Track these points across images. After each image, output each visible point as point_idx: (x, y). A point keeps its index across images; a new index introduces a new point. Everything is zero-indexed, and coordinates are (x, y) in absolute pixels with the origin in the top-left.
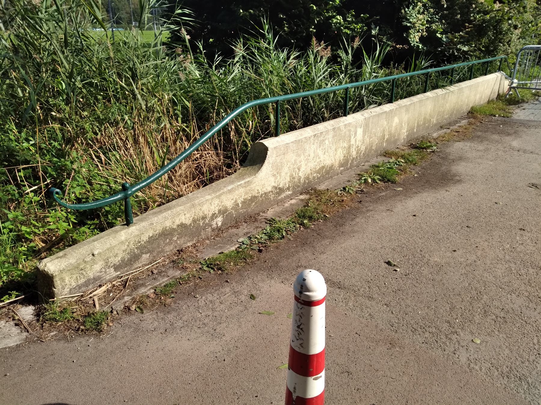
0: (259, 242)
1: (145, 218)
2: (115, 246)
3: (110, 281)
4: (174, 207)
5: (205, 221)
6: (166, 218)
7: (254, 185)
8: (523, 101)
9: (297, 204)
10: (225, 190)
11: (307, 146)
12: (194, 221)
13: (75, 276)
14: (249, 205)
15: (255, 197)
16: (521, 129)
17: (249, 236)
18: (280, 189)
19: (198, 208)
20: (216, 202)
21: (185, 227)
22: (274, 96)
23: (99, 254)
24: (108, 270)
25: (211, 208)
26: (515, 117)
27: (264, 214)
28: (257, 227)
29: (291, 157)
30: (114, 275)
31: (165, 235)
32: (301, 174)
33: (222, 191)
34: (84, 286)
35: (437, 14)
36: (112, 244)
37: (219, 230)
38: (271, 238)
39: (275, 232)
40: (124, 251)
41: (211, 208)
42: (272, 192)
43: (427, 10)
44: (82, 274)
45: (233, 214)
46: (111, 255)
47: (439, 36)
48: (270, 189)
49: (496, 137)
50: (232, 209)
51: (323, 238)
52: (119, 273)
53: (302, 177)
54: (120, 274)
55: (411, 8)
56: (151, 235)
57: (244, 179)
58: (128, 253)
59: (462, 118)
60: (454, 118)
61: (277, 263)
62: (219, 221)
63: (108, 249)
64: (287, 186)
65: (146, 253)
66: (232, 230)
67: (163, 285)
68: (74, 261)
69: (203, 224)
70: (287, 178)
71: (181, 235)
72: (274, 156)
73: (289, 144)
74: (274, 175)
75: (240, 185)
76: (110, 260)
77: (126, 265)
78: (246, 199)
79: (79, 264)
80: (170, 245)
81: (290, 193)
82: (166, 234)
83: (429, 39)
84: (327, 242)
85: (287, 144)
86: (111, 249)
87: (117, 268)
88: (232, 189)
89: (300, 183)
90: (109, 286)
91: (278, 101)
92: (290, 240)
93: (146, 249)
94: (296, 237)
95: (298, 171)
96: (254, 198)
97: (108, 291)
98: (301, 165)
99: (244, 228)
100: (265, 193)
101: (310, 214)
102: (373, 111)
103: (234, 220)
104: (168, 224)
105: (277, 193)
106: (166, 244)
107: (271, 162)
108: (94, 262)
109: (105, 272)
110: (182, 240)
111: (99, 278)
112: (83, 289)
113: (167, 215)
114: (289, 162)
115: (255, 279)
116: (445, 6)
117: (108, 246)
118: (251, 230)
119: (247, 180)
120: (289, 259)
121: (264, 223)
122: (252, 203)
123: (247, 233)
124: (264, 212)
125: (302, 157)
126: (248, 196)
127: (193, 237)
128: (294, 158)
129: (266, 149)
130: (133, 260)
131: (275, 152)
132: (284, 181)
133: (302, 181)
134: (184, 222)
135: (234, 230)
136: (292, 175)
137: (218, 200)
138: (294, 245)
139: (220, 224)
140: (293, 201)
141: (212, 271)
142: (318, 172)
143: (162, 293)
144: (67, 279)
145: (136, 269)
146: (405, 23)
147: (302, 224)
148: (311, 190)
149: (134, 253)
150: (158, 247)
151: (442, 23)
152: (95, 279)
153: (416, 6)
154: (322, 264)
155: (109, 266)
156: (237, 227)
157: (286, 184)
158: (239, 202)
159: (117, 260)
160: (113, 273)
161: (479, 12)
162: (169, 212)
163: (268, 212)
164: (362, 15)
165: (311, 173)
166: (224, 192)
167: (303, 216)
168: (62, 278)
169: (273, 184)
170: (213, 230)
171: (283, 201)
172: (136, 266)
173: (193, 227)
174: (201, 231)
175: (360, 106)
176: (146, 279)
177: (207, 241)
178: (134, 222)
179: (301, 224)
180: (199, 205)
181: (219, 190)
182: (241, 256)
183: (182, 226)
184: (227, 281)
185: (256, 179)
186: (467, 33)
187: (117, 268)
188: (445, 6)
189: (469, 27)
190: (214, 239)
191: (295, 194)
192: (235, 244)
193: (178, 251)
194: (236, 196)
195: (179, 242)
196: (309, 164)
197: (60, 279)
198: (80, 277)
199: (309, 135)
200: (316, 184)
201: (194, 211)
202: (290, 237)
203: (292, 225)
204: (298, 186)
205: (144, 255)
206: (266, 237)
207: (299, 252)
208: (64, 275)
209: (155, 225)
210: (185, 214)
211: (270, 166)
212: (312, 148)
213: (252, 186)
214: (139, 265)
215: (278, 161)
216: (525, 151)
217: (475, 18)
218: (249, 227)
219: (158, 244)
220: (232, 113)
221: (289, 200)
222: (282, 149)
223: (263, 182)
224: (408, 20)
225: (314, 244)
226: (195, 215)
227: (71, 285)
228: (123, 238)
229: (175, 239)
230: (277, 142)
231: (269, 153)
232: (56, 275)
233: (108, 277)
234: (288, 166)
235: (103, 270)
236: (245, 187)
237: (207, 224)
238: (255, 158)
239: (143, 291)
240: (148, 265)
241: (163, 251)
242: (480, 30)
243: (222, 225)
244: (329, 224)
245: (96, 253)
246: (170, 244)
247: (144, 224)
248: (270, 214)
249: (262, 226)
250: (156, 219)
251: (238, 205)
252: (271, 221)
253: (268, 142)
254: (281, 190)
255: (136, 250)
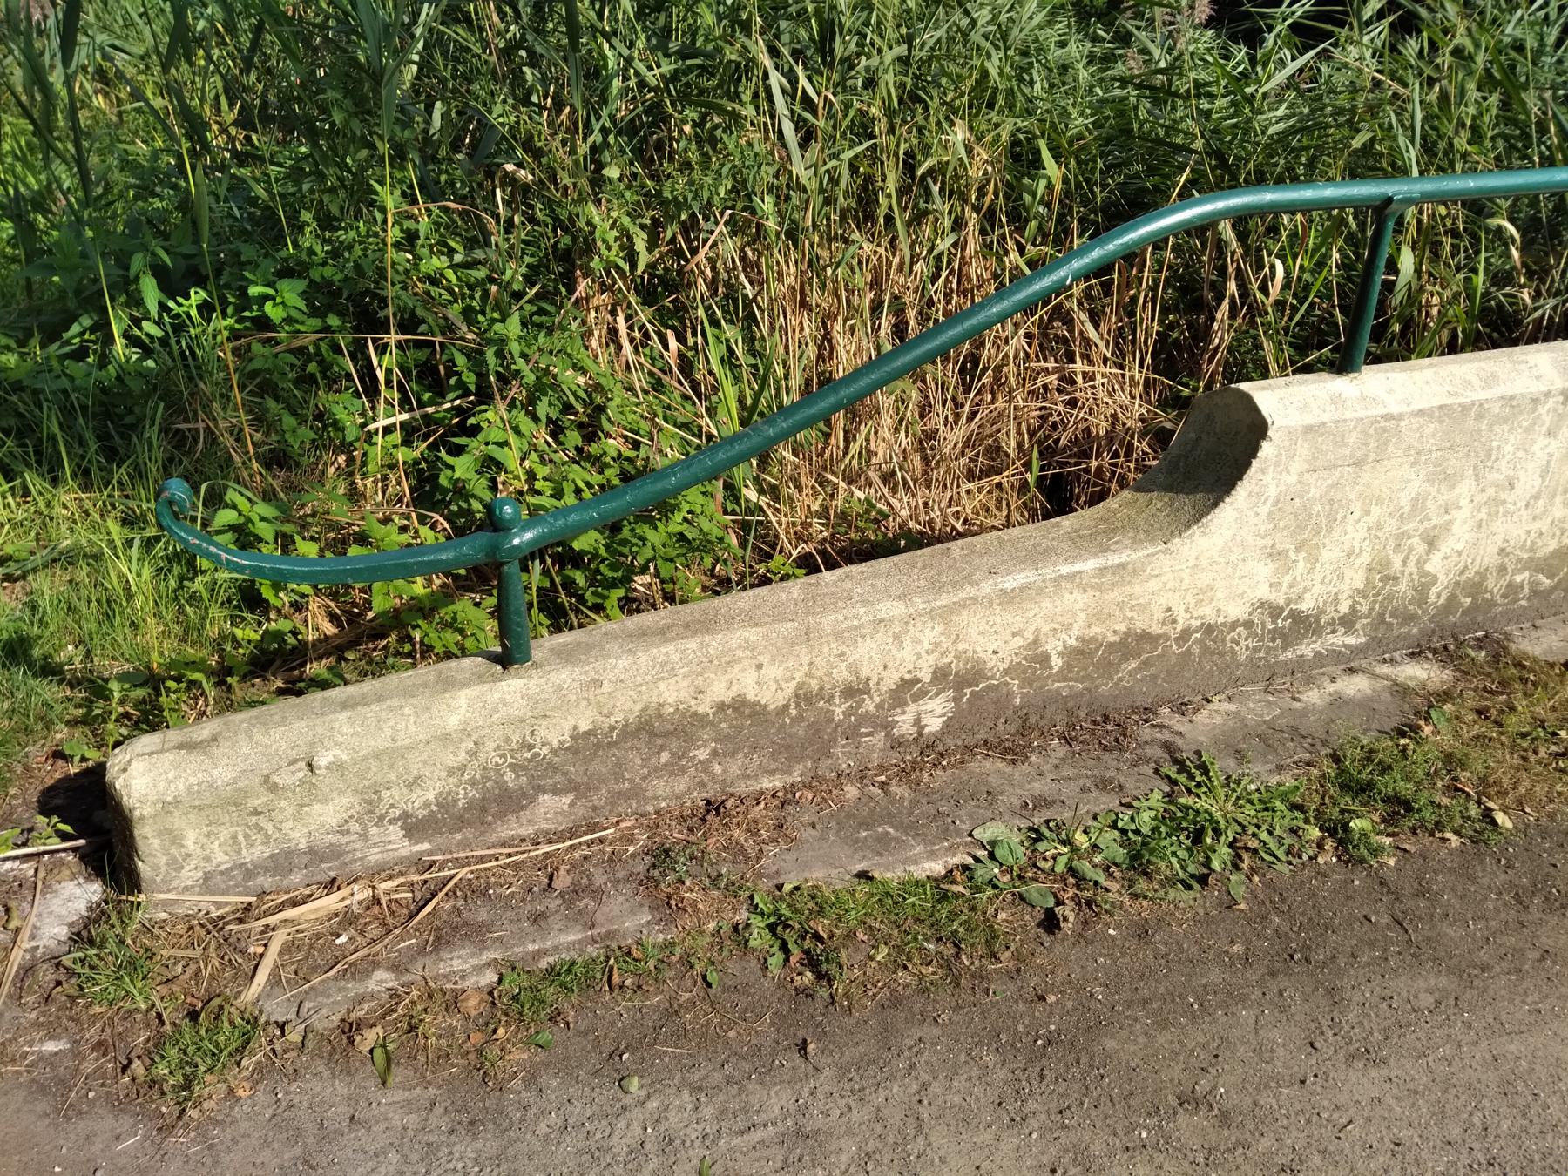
0: (1072, 870)
1: (588, 648)
2: (410, 748)
3: (374, 874)
4: (729, 623)
5: (860, 703)
6: (666, 670)
7: (1153, 585)
9: (1366, 705)
10: (987, 587)
11: (1508, 443)
12: (804, 697)
13: (224, 834)
14: (1107, 667)
15: (1146, 637)
17: (1037, 820)
18: (1296, 616)
19: (829, 649)
20: (930, 634)
21: (754, 714)
22: (908, 224)
23: (337, 767)
24: (374, 830)
25: (900, 655)
27: (1176, 722)
28: (1103, 784)
29: (1400, 480)
30: (404, 853)
31: (652, 734)
32: (1435, 565)
33: (968, 591)
34: (266, 869)
36: (401, 735)
37: (930, 750)
38: (1139, 861)
39: (1182, 834)
40: (451, 771)
41: (900, 655)
42: (1248, 624)
44: (259, 828)
45: (1010, 695)
46: (393, 777)
48: (1237, 611)
50: (1006, 672)
51: (1415, 956)
52: (426, 846)
53: (1443, 580)
54: (430, 853)
56: (584, 726)
57: (1105, 550)
58: (472, 782)
61: (1096, 1027)
63: (377, 756)
64: (1344, 608)
65: (556, 791)
66: (987, 764)
67: (543, 964)
68: (229, 775)
69: (847, 714)
70: (1348, 574)
71: (729, 746)
72: (1297, 466)
73: (1400, 417)
74: (1275, 555)
75: (1071, 577)
76: (385, 794)
77: (460, 822)
78: (1093, 639)
79: (244, 793)
80: (672, 774)
81: (1351, 640)
82: (657, 732)
84: (1423, 986)
85: (1387, 417)
86: (393, 755)
87: (414, 828)
88: (1024, 588)
89: (1421, 599)
90: (358, 897)
91: (1389, 201)
92: (1231, 904)
93: (558, 777)
94: (1276, 898)
95: (1421, 548)
96: (1136, 643)
97: (348, 919)
98: (1447, 527)
99: (1044, 774)
100: (1209, 629)
101: (1406, 789)
103: (1005, 723)
104: (672, 694)
105: (1275, 634)
106: (656, 769)
107: (1272, 491)
108: (310, 792)
109: (364, 836)
110: (735, 766)
111: (335, 853)
112: (265, 881)
113: (675, 658)
114: (1380, 502)
115: (936, 1088)
117: (382, 742)
118: (1069, 791)
119: (1113, 559)
120: (1164, 1025)
121: (1148, 770)
122: (1125, 658)
123: (1042, 802)
124: (1181, 708)
125: (1465, 489)
126: (1111, 631)
127: (793, 760)
128: (1416, 486)
129: (1257, 428)
130: (494, 808)
131: (1304, 450)
132: (1332, 578)
133: (1437, 595)
134: (751, 696)
135: (992, 767)
136: (1388, 563)
137: (939, 628)
138: (1238, 948)
139: (933, 725)
140: (1355, 686)
141: (775, 961)
142: (1546, 566)
143: (527, 1000)
144: (191, 839)
145: (503, 844)
147: (1337, 831)
148: (1480, 644)
149: (501, 784)
150: (618, 776)
152: (315, 854)
154: (1328, 1132)
155: (381, 818)
156: (1013, 752)
157: (1336, 601)
158: (1053, 647)
159: (420, 801)
160: (396, 844)
162: (693, 644)
163: (1202, 717)
165: (1502, 569)
166: (974, 599)
167: (1359, 783)
168: (169, 832)
169: (1264, 592)
170: (896, 744)
171: (1304, 672)
172: (505, 831)
173: (797, 720)
174: (833, 741)
176: (508, 906)
177: (851, 791)
178: (537, 654)
179: (1332, 832)
180: (838, 635)
181: (956, 586)
182: (945, 924)
183: (740, 707)
184: (803, 1047)
185: (1164, 562)
187: (414, 828)
190: (883, 786)
191: (1380, 647)
192: (952, 850)
193: (708, 802)
194: (1038, 622)
195: (718, 769)
196: (1499, 526)
197: (159, 834)
198: (247, 836)
199: (1536, 388)
200: (1518, 617)
201: (805, 660)
202: (1239, 891)
203: (1283, 818)
204: (1409, 618)
205: (545, 799)
206: (1120, 854)
207: (1243, 999)
208: (177, 821)
209: (606, 687)
210: (759, 667)
211: (1265, 509)
212: (1528, 458)
213: (1137, 589)
214: (523, 832)
215: (1314, 492)
218: (1067, 771)
219: (619, 764)
220: (1135, 243)
221: (1336, 670)
222: (1353, 438)
223: (1205, 579)
225: (1346, 982)
226: (809, 675)
227: (208, 859)
228: (453, 721)
229: (703, 754)
230: (1336, 400)
231: (1267, 449)
232: (142, 818)
233: (375, 856)
234: (1370, 519)
235: (356, 827)
236: (1098, 588)
237: (866, 719)
238: (1205, 457)
239: (457, 965)
240: (560, 837)
241: (637, 793)
243: (946, 729)
244: (1491, 875)
245: (322, 761)
246: (675, 769)
247: (566, 677)
248: (1203, 727)
249: (1130, 785)
250: (624, 662)
251: (1045, 659)
252: (1188, 768)
253: (1284, 400)
254: (1303, 624)
255: (509, 776)
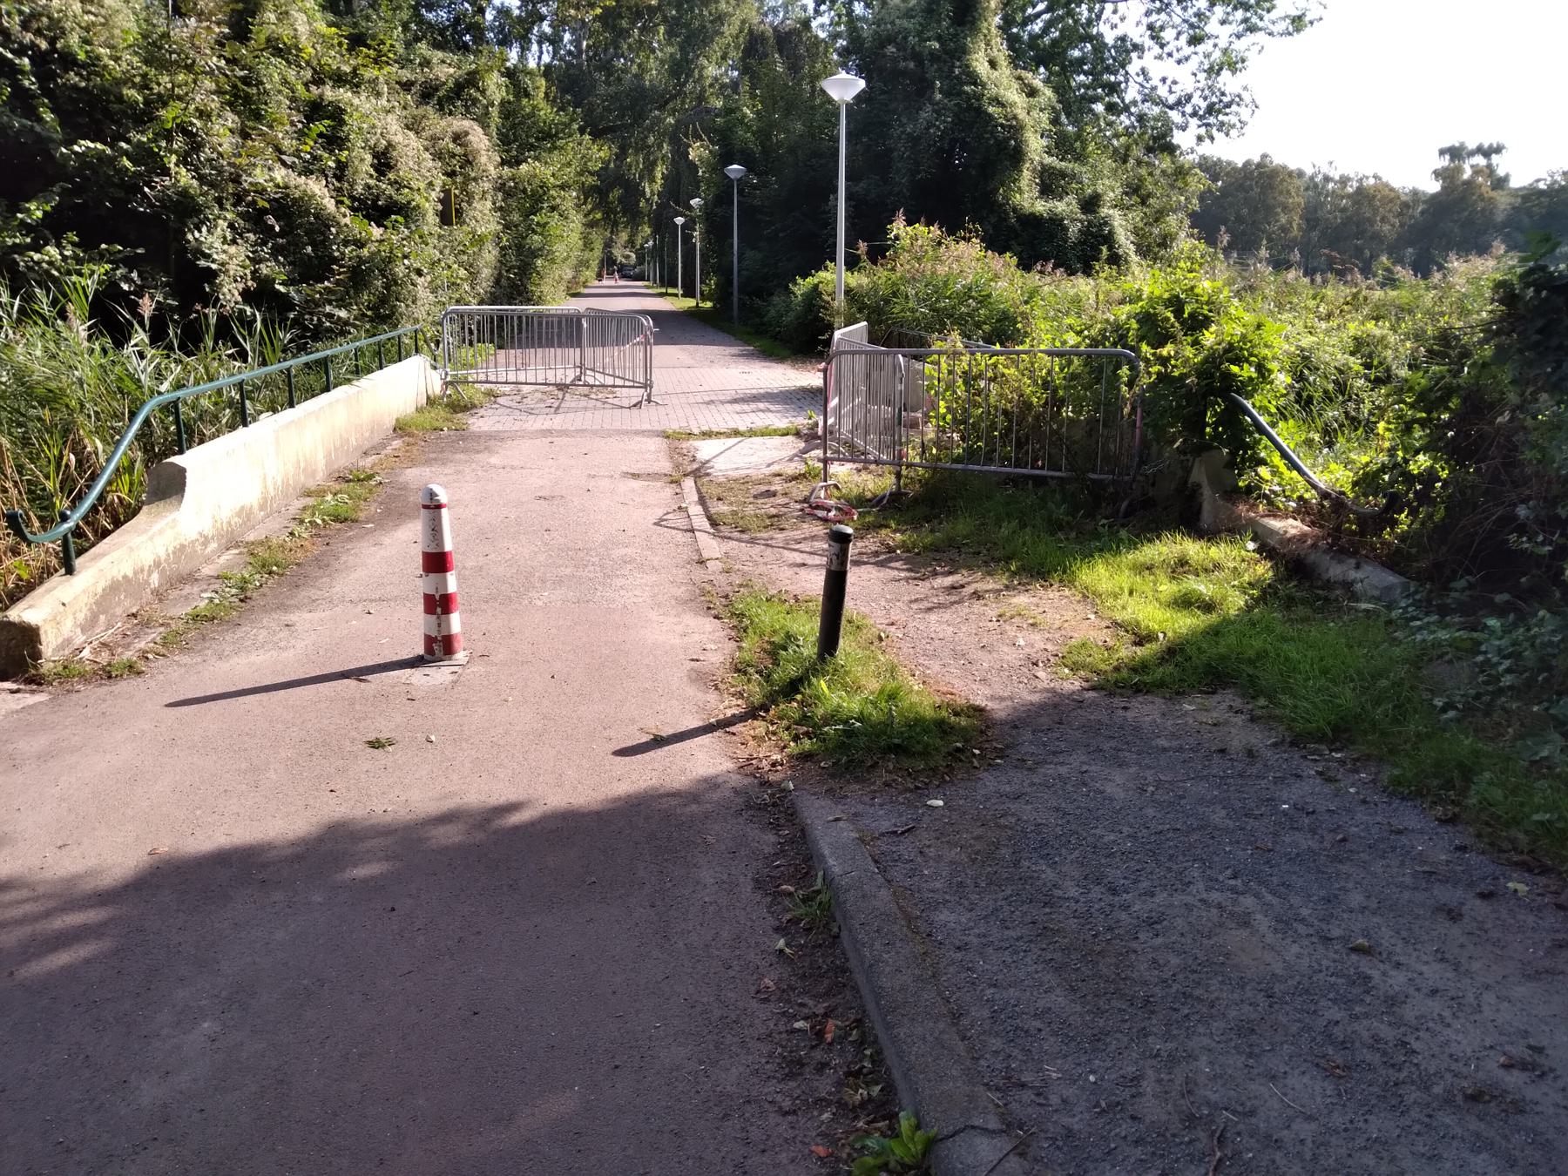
8: (474, 406)
16: (492, 443)
26: (473, 428)
35: (264, 243)
43: (241, 235)
47: (282, 289)
49: (461, 456)
55: (204, 229)
59: (389, 440)
60: (377, 440)
62: (155, 580)
83: (261, 293)
102: (267, 426)
116: (277, 229)
146: (202, 263)
151: (277, 261)
153: (216, 226)
161: (346, 243)
164: (103, 246)
175: (242, 418)
186: (338, 283)
188: (277, 229)
189: (340, 273)
216: (513, 468)
217: (343, 254)
224: (207, 257)
242: (358, 277)
